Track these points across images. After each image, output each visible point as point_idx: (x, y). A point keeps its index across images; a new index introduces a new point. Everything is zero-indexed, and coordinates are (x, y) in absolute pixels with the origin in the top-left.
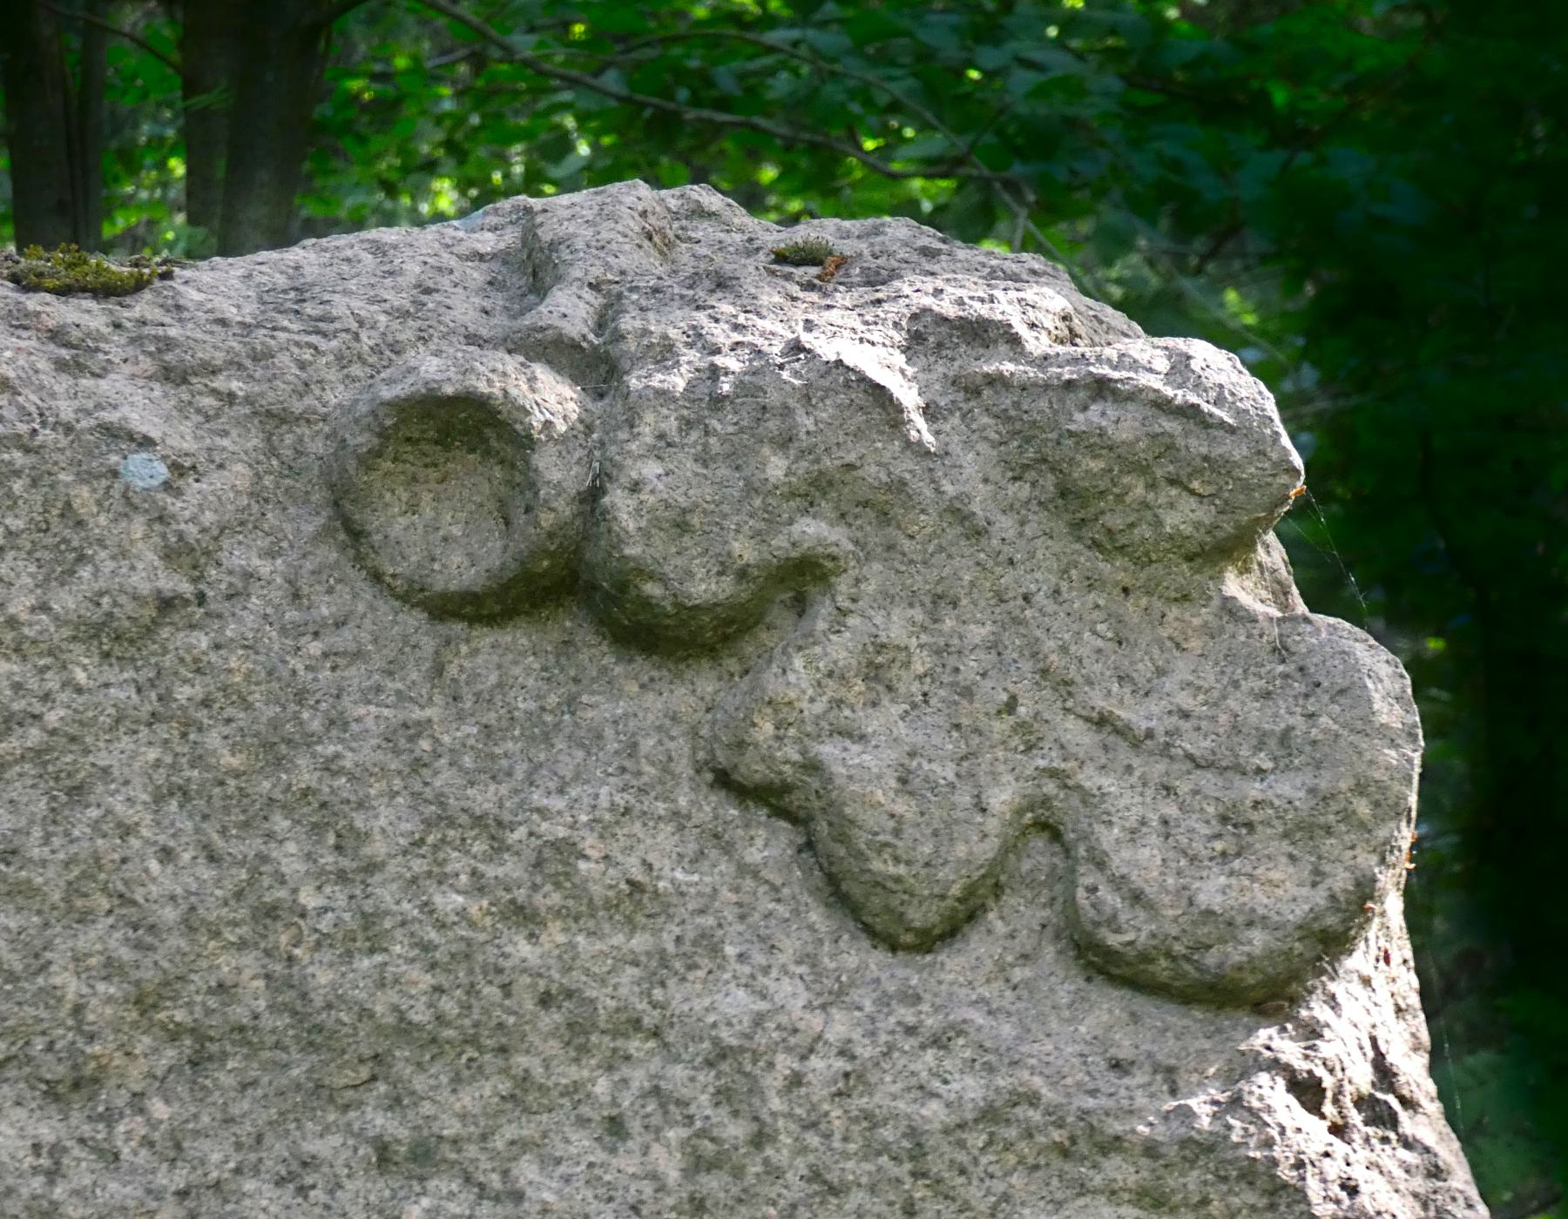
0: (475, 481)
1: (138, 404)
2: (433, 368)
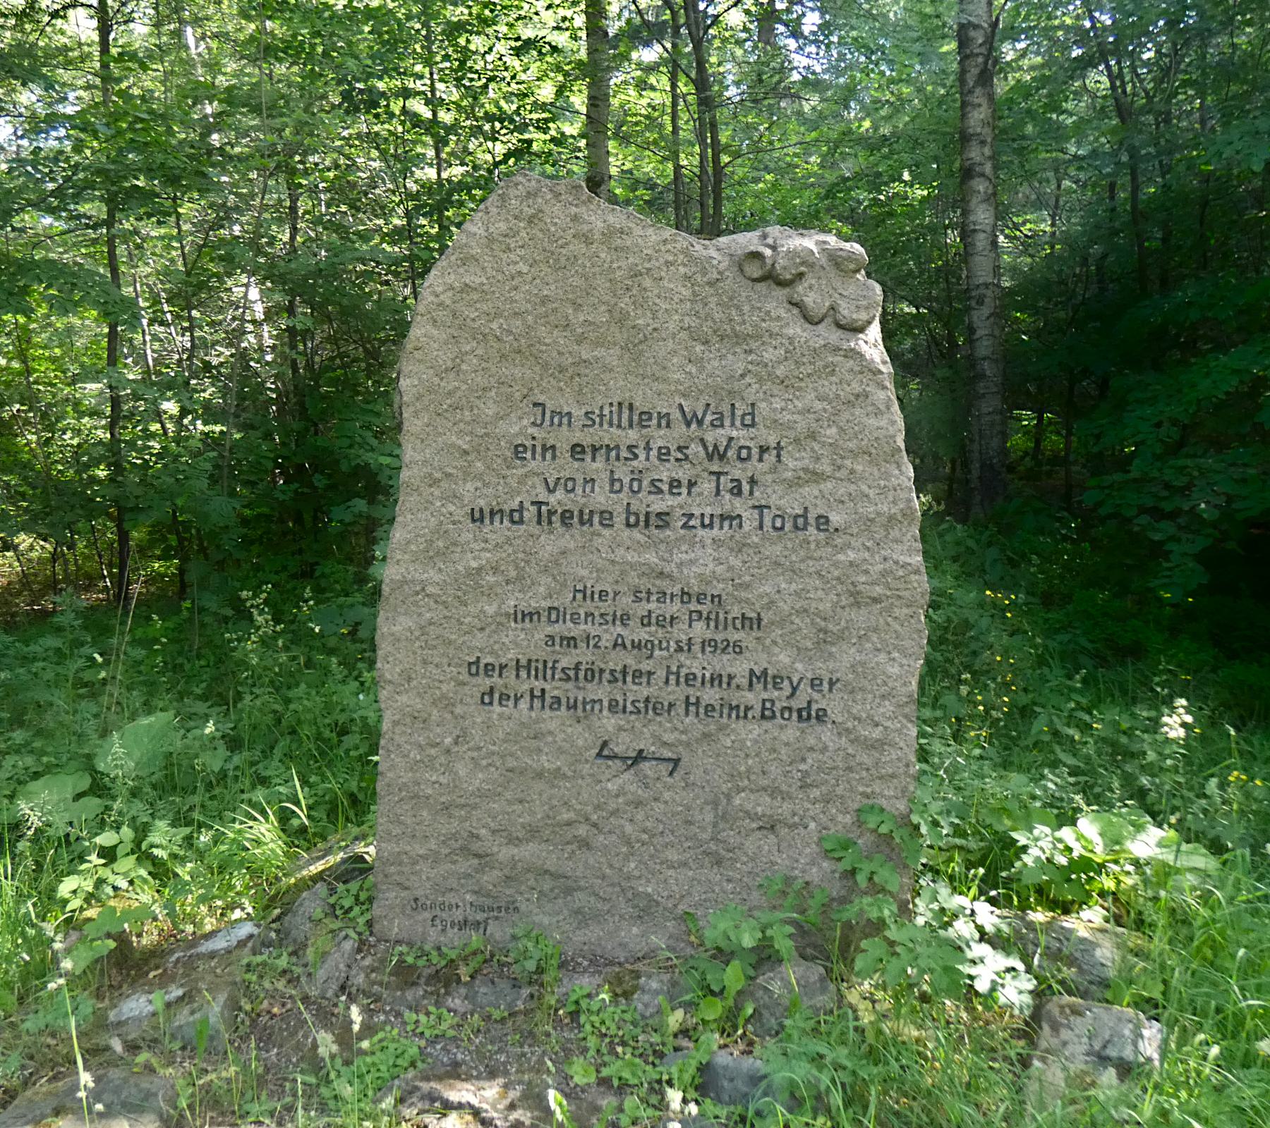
0: (757, 263)
1: (714, 253)
2: (752, 248)
